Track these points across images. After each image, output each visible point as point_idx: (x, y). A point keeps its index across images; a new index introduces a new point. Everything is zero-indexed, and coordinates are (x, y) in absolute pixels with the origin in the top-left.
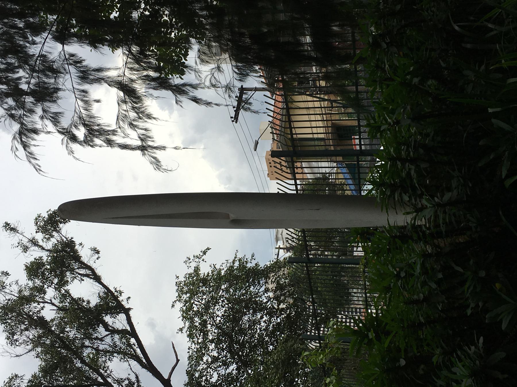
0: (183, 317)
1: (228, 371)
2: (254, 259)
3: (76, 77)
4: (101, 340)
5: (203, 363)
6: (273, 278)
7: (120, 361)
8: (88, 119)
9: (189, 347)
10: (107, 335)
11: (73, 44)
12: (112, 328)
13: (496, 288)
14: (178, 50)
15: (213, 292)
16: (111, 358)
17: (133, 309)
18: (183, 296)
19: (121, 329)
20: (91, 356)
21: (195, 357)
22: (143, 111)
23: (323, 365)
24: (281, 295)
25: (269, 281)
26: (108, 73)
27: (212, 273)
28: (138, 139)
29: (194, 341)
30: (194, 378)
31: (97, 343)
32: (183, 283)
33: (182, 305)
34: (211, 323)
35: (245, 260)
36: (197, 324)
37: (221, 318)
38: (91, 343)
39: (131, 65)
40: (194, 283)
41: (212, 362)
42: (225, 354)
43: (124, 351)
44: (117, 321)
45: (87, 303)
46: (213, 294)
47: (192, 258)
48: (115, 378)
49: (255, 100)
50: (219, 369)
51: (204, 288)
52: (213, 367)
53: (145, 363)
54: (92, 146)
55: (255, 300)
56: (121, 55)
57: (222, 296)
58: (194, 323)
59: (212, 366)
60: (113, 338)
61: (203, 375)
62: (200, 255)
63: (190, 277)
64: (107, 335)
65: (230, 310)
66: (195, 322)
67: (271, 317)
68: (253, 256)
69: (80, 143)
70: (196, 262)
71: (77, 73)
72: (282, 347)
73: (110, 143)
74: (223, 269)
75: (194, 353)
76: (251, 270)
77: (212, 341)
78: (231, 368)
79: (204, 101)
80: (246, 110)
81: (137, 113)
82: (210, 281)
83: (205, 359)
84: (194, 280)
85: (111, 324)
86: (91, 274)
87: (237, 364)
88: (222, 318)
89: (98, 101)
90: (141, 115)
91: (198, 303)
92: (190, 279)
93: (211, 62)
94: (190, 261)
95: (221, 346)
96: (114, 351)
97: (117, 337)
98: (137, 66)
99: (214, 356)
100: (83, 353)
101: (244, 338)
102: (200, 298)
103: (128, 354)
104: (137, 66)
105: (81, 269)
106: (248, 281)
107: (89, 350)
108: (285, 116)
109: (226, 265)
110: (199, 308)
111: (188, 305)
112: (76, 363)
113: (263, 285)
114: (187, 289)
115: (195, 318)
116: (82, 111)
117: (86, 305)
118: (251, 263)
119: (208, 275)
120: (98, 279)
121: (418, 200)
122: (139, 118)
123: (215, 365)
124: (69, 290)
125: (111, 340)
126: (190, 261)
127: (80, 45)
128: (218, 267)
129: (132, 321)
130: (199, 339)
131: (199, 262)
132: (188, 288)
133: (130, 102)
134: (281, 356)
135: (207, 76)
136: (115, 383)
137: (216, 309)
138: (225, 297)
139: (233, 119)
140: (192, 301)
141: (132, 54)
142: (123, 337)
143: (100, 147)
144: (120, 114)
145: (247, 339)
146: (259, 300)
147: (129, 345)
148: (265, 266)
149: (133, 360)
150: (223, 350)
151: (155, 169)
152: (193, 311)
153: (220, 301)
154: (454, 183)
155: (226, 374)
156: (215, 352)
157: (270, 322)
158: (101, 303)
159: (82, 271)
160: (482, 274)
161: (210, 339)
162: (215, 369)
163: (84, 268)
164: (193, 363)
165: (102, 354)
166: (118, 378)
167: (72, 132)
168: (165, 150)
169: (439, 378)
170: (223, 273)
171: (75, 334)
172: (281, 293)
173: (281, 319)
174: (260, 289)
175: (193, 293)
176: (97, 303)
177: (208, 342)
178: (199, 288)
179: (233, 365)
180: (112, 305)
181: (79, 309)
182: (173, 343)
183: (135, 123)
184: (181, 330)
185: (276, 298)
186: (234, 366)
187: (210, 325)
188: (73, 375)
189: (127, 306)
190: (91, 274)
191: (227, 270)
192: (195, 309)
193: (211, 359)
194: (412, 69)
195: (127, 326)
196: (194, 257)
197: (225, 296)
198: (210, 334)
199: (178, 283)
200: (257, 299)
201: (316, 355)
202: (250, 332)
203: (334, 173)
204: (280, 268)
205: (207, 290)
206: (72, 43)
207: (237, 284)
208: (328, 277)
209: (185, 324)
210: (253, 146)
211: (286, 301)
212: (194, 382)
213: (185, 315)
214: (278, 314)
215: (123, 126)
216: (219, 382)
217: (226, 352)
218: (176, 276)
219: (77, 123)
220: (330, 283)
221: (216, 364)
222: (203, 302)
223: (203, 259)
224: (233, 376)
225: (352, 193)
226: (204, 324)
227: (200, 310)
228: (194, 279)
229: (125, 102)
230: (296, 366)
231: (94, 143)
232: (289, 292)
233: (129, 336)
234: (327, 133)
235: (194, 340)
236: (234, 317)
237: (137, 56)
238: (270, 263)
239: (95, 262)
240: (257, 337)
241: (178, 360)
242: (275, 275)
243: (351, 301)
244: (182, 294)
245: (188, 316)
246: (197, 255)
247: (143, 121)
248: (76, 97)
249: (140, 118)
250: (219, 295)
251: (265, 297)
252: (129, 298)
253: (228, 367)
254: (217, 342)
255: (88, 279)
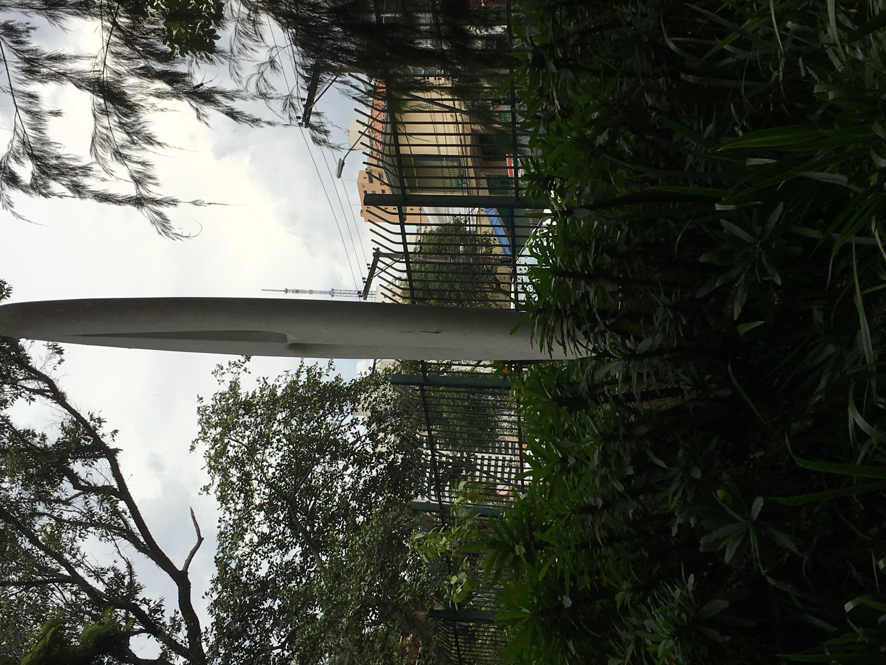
0: (211, 467)
1: (287, 558)
2: (333, 370)
3: (17, 70)
4: (67, 503)
5: (244, 544)
6: (366, 402)
7: (100, 539)
8: (39, 146)
9: (220, 518)
10: (77, 496)
11: (11, 8)
12: (86, 483)
13: (717, 496)
14: (205, 7)
15: (263, 424)
16: (83, 533)
17: (122, 450)
18: (209, 432)
19: (101, 485)
20: (49, 529)
21: (231, 534)
22: (140, 130)
23: (446, 554)
24: (379, 430)
25: (358, 407)
26: (75, 64)
27: (261, 391)
28: (130, 179)
29: (229, 508)
30: (229, 569)
31: (59, 508)
32: (211, 409)
33: (208, 446)
34: (259, 477)
35: (318, 370)
36: (234, 479)
37: (275, 468)
38: (48, 508)
39: (117, 47)
40: (229, 410)
41: (259, 544)
42: (282, 530)
43: (107, 523)
44: (94, 471)
45: (41, 440)
46: (263, 428)
47: (226, 366)
48: (90, 567)
49: (334, 128)
50: (272, 554)
51: (246, 418)
52: (260, 552)
53: (143, 543)
54: (46, 196)
55: (335, 438)
56: (98, 29)
57: (278, 431)
58: (229, 477)
59: (259, 550)
60: (87, 500)
61: (244, 564)
62: (239, 361)
63: (223, 399)
64: (77, 496)
65: (292, 456)
66: (231, 475)
67: (361, 466)
68: (332, 365)
69: (24, 189)
70: (232, 372)
71: (17, 62)
72: (378, 520)
73: (78, 189)
74: (280, 386)
75: (229, 528)
76: (328, 387)
77: (260, 508)
78: (292, 553)
79: (247, 117)
80: (319, 143)
81: (128, 133)
82: (258, 407)
83: (247, 537)
84: (229, 404)
85: (83, 477)
86: (49, 389)
87: (302, 545)
88: (278, 470)
89: (57, 114)
90: (135, 138)
91: (236, 444)
92: (223, 403)
93: (257, 50)
94: (222, 371)
95: (275, 515)
96: (90, 521)
97: (93, 499)
98: (126, 50)
99: (262, 533)
100: (34, 526)
101: (315, 502)
102: (240, 434)
103: (115, 528)
104: (128, 49)
105: (30, 381)
106: (322, 407)
107: (45, 520)
108: (389, 136)
109: (286, 379)
110: (238, 452)
111: (219, 447)
112: (22, 543)
113: (349, 413)
114: (217, 419)
115: (230, 469)
116: (28, 131)
117: (39, 443)
118: (328, 375)
119: (254, 396)
120: (60, 398)
121: (600, 339)
122: (132, 144)
123: (264, 548)
124: (9, 417)
125: (84, 504)
126: (222, 371)
127: (23, 12)
128: (270, 382)
129: (121, 472)
130: (237, 503)
131: (239, 373)
132: (220, 417)
133: (116, 115)
134: (376, 535)
135: (252, 76)
136: (91, 576)
137: (268, 454)
138: (284, 434)
139: (300, 121)
140: (226, 441)
141: (119, 28)
142: (105, 499)
143: (61, 197)
144: (98, 134)
145: (320, 504)
146: (341, 438)
147: (116, 513)
148: (352, 381)
149: (123, 539)
150: (279, 523)
151: (161, 234)
152: (228, 457)
153: (274, 440)
154: (659, 317)
155: (284, 563)
156: (265, 526)
157: (360, 476)
158: (67, 440)
159: (33, 384)
160: (697, 474)
161: (257, 504)
162: (265, 555)
163: (35, 379)
164: (227, 544)
165: (68, 526)
166: (97, 568)
167: (9, 168)
168: (175, 205)
169: (623, 627)
170: (279, 393)
171: (20, 494)
172: (379, 427)
173: (379, 471)
174: (342, 420)
175: (227, 427)
176: (59, 439)
177: (253, 509)
178: (237, 417)
179: (295, 548)
180: (85, 444)
181: (28, 449)
182: (192, 510)
183: (125, 152)
184: (206, 489)
185: (372, 436)
186: (298, 549)
187: (257, 482)
188: (16, 562)
189: (112, 446)
190: (49, 389)
191: (286, 387)
192: (231, 453)
193: (259, 539)
194: (596, 115)
195: (111, 480)
196: (230, 364)
197: (283, 432)
198: (256, 496)
199: (201, 409)
200: (338, 438)
201: (435, 538)
202: (326, 492)
203: (474, 215)
204: (377, 385)
205: (251, 422)
206: (9, 8)
207: (304, 411)
208: (460, 395)
209: (213, 478)
210: (335, 167)
211: (387, 441)
212: (228, 576)
213: (213, 463)
214: (373, 463)
215: (103, 156)
216: (270, 577)
217: (284, 525)
218: (198, 397)
219: (19, 153)
220: (463, 406)
221: (266, 546)
222: (245, 441)
223: (246, 368)
224: (296, 566)
225: (504, 251)
226: (246, 478)
227: (240, 455)
228: (229, 402)
229: (106, 113)
230: (402, 553)
231: (50, 190)
232: (391, 425)
233: (116, 497)
234: (463, 146)
235: (229, 506)
236: (298, 467)
237: (128, 31)
238: (360, 376)
239: (55, 369)
240: (337, 500)
241: (201, 539)
242: (368, 396)
243: (498, 435)
244: (209, 428)
245: (218, 466)
246: (235, 362)
247: (140, 148)
248: (16, 106)
249: (133, 143)
250: (272, 431)
251: (352, 433)
252: (116, 431)
253: (287, 552)
254: (269, 509)
255: (43, 398)
